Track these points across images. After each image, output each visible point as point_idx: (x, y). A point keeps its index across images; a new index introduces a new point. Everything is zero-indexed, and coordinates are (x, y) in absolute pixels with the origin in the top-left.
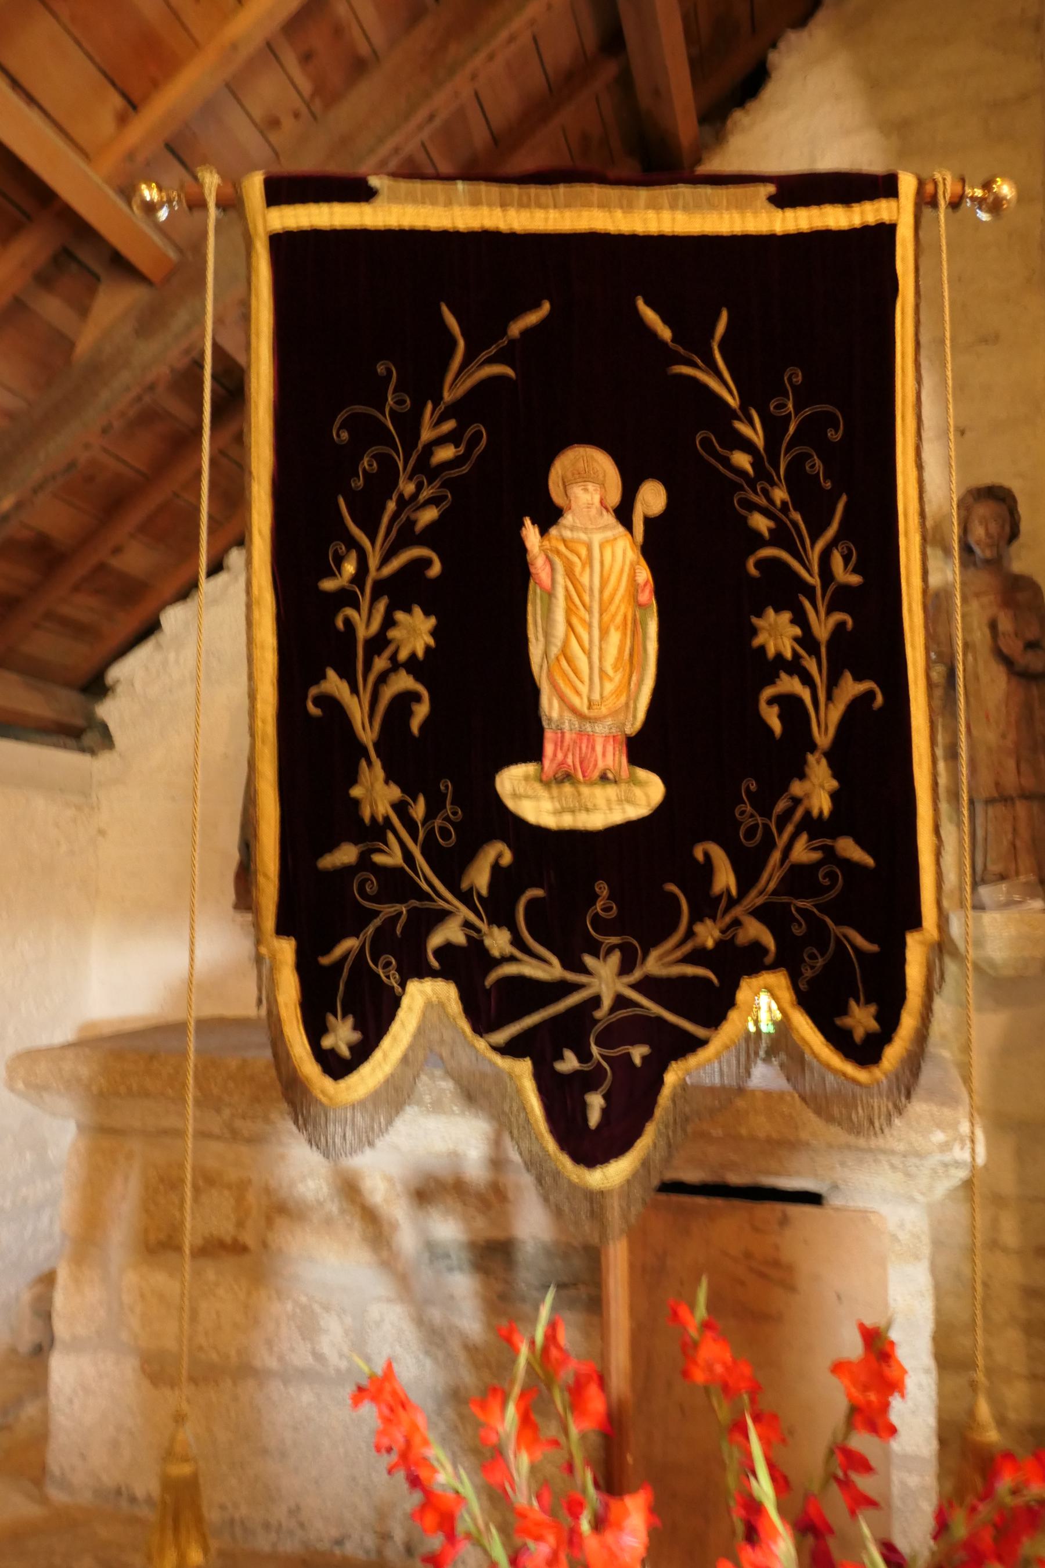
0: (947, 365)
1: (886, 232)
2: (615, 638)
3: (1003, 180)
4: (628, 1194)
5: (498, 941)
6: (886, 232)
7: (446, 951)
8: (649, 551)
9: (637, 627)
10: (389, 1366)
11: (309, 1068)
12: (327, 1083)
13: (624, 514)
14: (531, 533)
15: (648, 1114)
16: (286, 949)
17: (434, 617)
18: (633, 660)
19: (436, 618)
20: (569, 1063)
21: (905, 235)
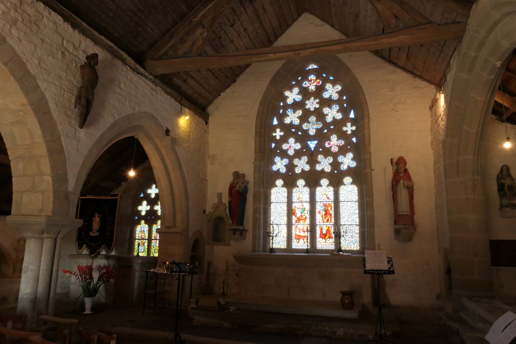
0: (55, 106)
1: (117, 199)
2: (97, 225)
3: (188, 120)
4: (195, 42)
5: (89, 242)
6: (117, 199)
7: (86, 243)
8: (100, 219)
9: (98, 224)
10: (167, 128)
11: (78, 249)
12: (79, 250)
13: (99, 217)
14: (93, 218)
15: (95, 252)
16: (77, 242)
17: (279, 139)
18: (98, 226)
19: (278, 140)
20: (91, 249)
21: (119, 199)
